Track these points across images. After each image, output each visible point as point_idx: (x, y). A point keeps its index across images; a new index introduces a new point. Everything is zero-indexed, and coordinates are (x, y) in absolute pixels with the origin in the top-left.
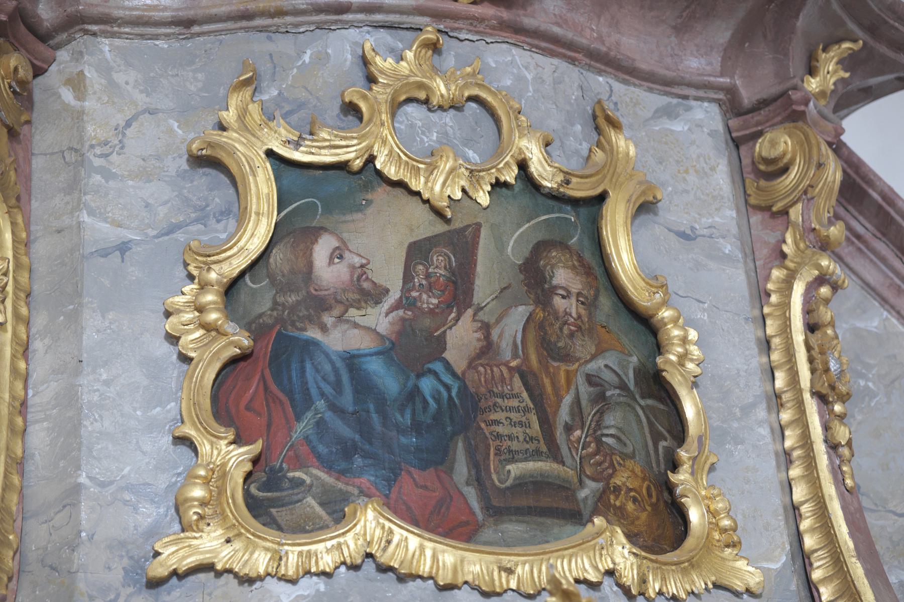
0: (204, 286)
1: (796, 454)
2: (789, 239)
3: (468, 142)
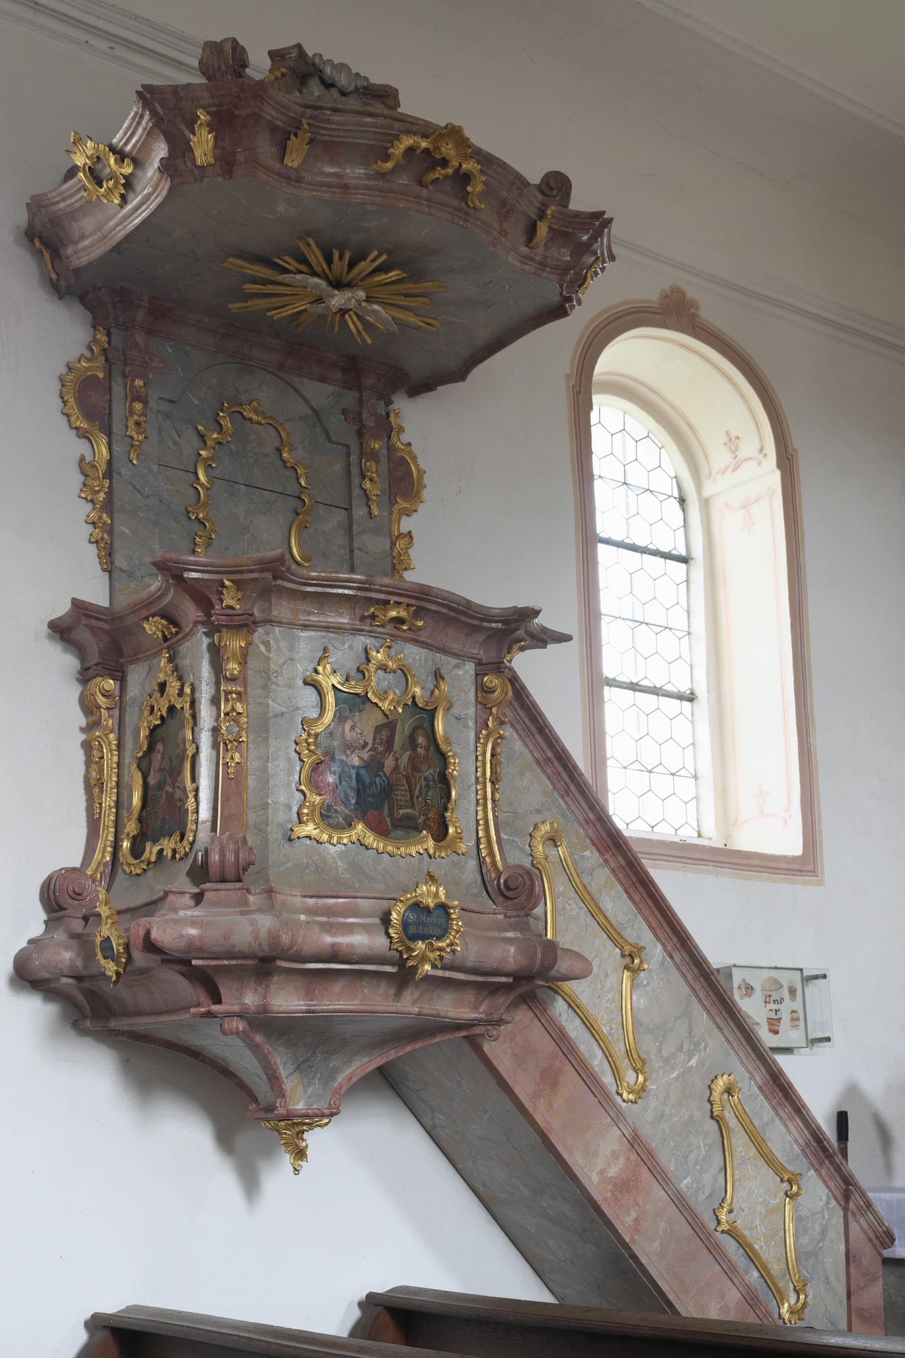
0: (309, 735)
1: (481, 801)
2: (490, 719)
3: (397, 686)
